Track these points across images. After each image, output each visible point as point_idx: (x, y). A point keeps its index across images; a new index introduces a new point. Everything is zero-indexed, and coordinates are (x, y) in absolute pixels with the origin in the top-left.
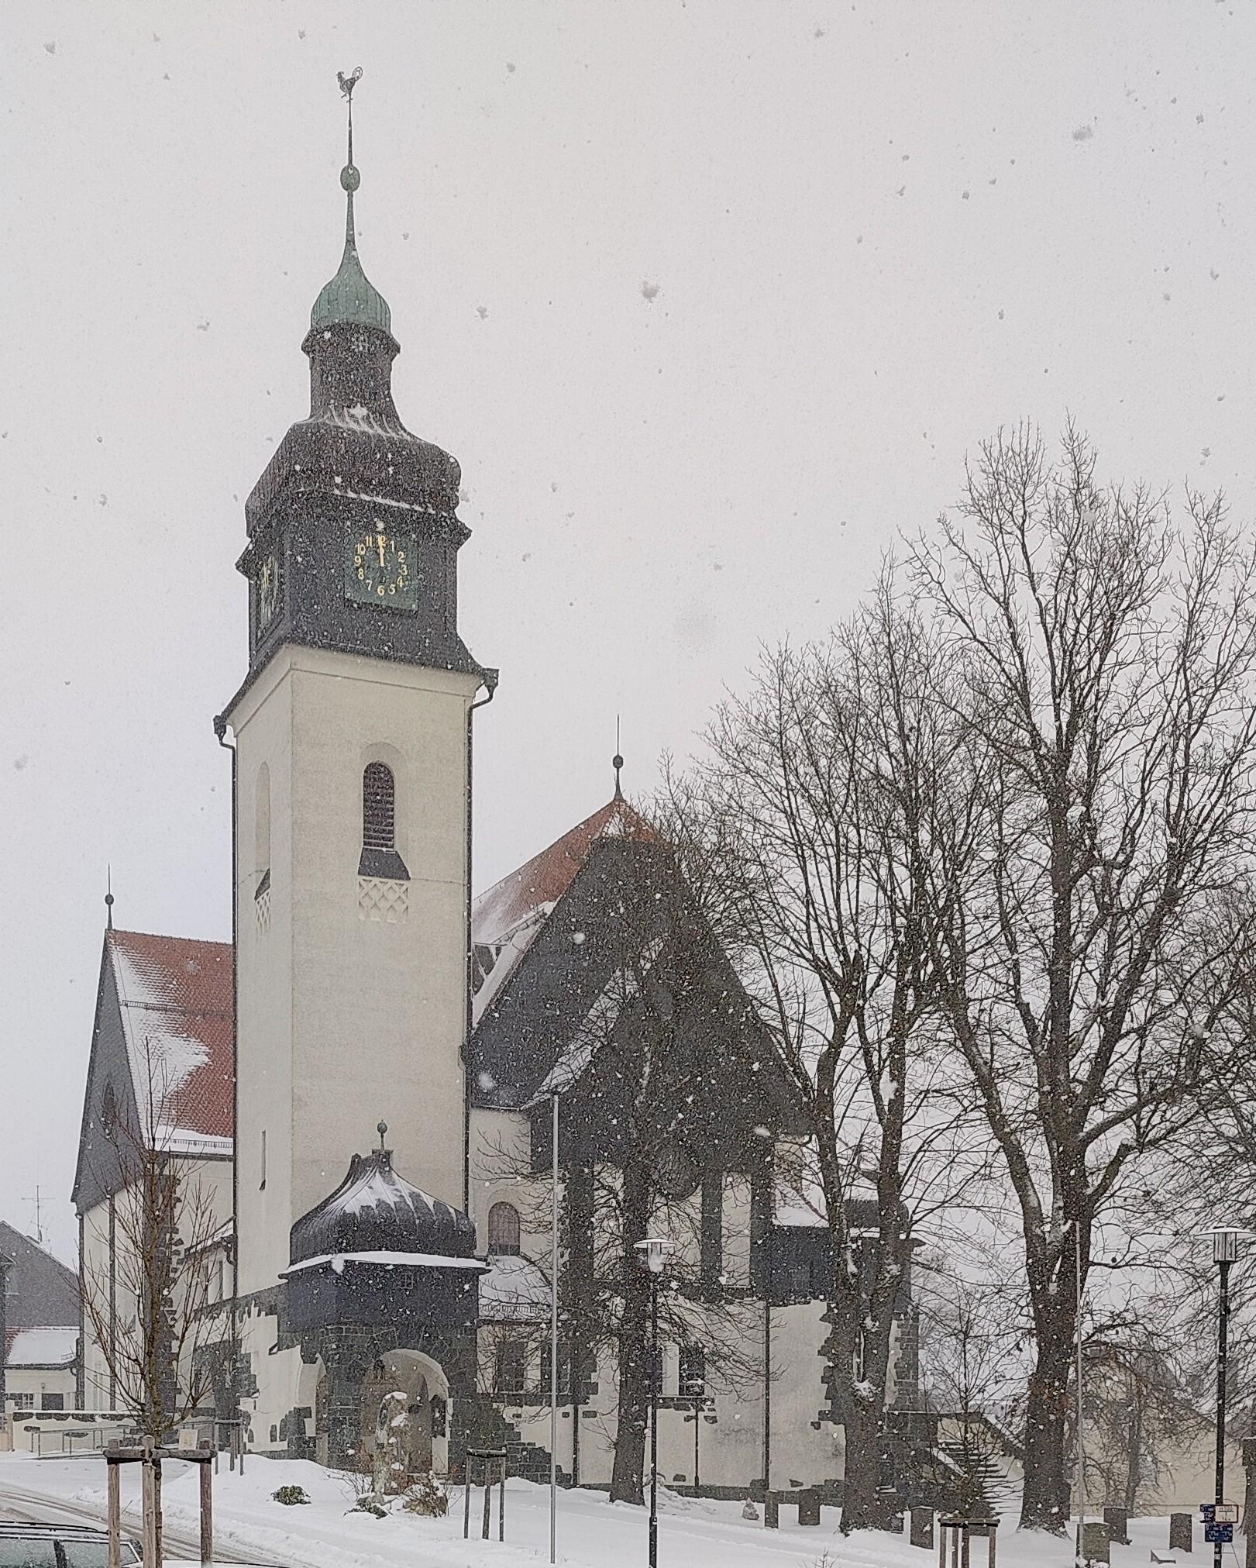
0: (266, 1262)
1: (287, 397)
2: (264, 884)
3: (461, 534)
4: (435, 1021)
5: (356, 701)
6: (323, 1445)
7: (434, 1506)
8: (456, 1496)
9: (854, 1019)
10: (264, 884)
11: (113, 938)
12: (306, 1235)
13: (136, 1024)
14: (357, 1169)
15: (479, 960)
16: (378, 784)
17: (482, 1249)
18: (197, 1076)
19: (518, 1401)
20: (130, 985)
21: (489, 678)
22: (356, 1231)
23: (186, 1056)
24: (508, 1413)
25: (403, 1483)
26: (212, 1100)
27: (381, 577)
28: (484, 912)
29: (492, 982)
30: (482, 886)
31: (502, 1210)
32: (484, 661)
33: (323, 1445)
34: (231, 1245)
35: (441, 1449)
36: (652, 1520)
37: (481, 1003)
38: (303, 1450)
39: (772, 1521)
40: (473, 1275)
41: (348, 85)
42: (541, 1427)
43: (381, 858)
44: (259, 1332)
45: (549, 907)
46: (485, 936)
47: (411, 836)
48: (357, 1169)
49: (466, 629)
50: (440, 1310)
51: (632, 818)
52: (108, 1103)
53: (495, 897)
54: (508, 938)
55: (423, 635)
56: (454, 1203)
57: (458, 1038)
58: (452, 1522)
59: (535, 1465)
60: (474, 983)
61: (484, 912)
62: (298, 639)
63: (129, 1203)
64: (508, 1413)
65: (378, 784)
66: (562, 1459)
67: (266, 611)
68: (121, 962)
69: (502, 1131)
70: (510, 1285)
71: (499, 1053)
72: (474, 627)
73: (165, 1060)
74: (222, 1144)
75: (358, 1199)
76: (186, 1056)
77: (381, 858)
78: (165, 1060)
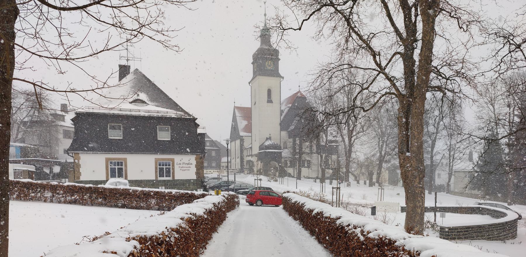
0: (256, 150)
1: (257, 45)
2: (255, 104)
3: (280, 59)
4: (277, 120)
5: (266, 82)
6: (263, 173)
7: (276, 181)
8: (278, 179)
9: (404, 35)
10: (255, 104)
11: (235, 107)
12: (261, 148)
13: (238, 119)
14: (267, 139)
15: (282, 112)
16: (269, 91)
17: (282, 148)
18: (246, 126)
19: (287, 167)
20: (238, 114)
21: (283, 78)
22: (268, 147)
23: (245, 123)
24: (285, 168)
25: (273, 178)
26: (248, 129)
27: (269, 66)
28: (283, 103)
29: (284, 114)
30: (283, 99)
31: (285, 143)
32: (282, 76)
33: (263, 173)
34: (251, 148)
35: (277, 174)
36: (436, 202)
37: (282, 117)
38: (261, 174)
39: (315, 182)
40: (281, 152)
41: (265, 3)
42: (290, 171)
43: (270, 101)
44: (254, 159)
45: (290, 105)
46: (282, 109)
47: (274, 97)
48: (267, 139)
49: (280, 72)
50: (277, 157)
51: (301, 94)
52: (234, 129)
53: (284, 102)
54: (285, 108)
55: (275, 73)
56: (279, 144)
57: (279, 122)
58: (278, 182)
59: (290, 175)
60: (281, 115)
61: (283, 103)
62: (260, 75)
63: (238, 142)
64: (285, 168)
65: (269, 91)
66: (292, 174)
67: (255, 70)
68: (236, 111)
69: (284, 134)
70: (286, 153)
71: (284, 125)
72: (281, 71)
73: (242, 124)
74: (250, 134)
75: (268, 143)
76: (245, 123)
77: (270, 101)
78: (242, 124)
